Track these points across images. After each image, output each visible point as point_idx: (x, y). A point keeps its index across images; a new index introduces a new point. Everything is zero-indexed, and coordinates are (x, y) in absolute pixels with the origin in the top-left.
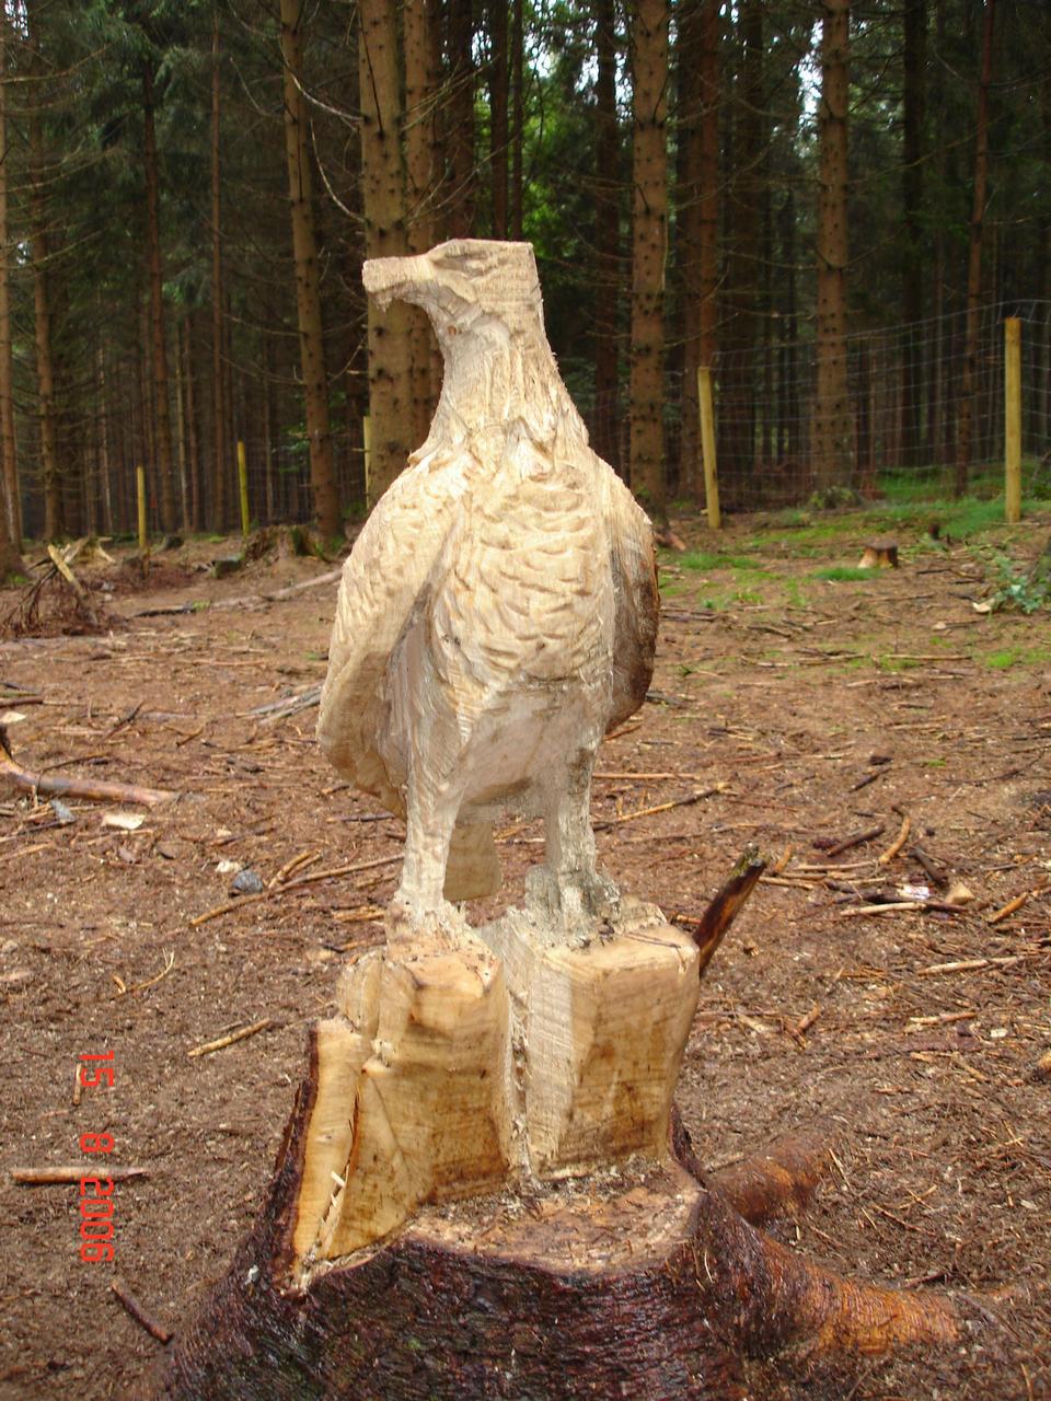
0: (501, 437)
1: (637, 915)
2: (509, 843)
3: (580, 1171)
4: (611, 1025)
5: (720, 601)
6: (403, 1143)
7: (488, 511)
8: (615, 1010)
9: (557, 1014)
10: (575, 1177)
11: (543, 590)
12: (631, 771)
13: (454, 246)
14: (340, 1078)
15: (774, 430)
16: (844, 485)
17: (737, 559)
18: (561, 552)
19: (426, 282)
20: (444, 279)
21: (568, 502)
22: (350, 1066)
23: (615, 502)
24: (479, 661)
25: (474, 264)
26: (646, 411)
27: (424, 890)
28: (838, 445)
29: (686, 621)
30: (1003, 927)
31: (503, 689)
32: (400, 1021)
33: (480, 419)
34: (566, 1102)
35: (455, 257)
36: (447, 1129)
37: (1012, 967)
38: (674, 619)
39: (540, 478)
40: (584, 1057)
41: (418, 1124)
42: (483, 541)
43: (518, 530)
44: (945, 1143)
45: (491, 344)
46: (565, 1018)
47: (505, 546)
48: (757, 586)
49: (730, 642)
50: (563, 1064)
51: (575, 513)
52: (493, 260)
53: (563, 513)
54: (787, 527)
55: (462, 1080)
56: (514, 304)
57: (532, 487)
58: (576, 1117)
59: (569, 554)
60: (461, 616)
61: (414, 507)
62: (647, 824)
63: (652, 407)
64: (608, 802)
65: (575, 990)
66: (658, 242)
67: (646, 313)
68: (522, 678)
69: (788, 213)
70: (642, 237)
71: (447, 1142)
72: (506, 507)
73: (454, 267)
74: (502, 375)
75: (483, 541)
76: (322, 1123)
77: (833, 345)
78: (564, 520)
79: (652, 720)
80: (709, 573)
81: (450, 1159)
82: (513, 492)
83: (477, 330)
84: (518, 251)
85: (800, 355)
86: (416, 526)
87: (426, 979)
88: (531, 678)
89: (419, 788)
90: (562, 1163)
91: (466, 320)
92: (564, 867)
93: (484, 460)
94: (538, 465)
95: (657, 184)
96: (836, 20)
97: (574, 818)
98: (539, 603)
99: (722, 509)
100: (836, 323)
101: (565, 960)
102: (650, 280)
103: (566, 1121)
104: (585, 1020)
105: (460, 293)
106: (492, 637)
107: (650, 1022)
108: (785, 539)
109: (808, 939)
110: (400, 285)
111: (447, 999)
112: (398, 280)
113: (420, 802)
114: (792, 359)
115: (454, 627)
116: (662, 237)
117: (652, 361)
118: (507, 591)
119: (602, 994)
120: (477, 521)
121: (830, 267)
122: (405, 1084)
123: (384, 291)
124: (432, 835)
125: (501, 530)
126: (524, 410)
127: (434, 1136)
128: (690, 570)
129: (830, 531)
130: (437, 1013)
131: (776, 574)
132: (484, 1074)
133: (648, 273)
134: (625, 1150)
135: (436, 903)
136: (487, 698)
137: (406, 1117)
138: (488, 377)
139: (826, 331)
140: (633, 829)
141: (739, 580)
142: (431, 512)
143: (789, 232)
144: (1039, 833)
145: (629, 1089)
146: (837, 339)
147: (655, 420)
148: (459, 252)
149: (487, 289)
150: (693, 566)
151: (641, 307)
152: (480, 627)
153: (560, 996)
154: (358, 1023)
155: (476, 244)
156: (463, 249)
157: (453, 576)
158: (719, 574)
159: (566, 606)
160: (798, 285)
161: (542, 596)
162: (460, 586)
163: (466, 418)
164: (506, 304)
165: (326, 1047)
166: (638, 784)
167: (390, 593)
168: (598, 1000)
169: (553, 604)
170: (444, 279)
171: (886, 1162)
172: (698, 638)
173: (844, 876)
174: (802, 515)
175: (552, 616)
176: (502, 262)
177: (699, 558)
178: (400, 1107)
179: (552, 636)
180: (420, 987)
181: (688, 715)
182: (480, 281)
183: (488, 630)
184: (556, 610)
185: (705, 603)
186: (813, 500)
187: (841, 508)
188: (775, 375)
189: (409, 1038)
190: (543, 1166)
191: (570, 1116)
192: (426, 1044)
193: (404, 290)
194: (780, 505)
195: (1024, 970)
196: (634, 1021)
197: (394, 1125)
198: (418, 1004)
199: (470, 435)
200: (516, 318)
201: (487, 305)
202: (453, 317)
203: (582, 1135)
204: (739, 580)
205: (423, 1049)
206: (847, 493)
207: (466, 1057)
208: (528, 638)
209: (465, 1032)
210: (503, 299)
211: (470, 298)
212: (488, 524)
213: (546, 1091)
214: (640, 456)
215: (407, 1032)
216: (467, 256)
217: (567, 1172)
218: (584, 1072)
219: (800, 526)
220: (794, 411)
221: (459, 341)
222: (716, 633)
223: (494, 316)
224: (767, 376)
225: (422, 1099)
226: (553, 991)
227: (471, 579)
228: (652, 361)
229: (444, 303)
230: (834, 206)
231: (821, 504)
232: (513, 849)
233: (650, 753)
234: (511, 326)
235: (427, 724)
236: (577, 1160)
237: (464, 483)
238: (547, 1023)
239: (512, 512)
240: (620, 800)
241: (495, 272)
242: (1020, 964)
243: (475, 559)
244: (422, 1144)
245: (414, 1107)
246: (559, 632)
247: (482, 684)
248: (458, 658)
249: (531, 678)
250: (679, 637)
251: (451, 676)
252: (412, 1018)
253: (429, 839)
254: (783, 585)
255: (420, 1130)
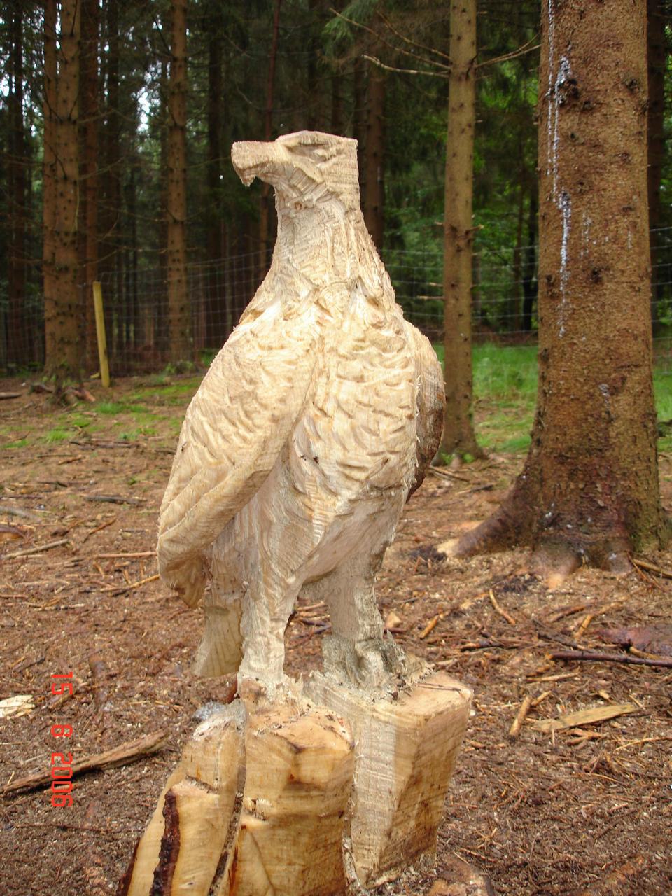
0: (346, 292)
1: (417, 667)
2: (57, 609)
3: (393, 877)
4: (424, 758)
5: (133, 435)
6: (275, 881)
7: (342, 351)
8: (428, 746)
9: (383, 755)
10: (390, 882)
11: (387, 415)
12: (123, 552)
13: (306, 136)
14: (200, 832)
15: (125, 325)
16: (186, 359)
17: (133, 406)
18: (397, 384)
19: (283, 164)
20: (297, 162)
21: (398, 346)
22: (208, 821)
23: (419, 347)
24: (332, 474)
25: (320, 152)
26: (66, 309)
27: (272, 667)
28: (183, 334)
29: (112, 448)
30: (431, 640)
31: (353, 497)
32: (279, 781)
33: (322, 275)
34: (387, 823)
35: (306, 145)
36: (313, 864)
37: (452, 667)
38: (103, 447)
39: (377, 326)
40: (403, 787)
41: (290, 864)
42: (339, 376)
43: (369, 367)
44: (484, 796)
45: (331, 217)
46: (389, 758)
47: (360, 379)
48: (152, 424)
49: (146, 462)
50: (385, 795)
51: (403, 354)
52: (333, 150)
53: (395, 353)
54: (155, 386)
55: (327, 822)
56: (348, 186)
57: (374, 332)
58: (393, 834)
59: (403, 386)
60: (319, 437)
61: (282, 347)
62: (152, 588)
63: (70, 307)
64: (117, 574)
65: (400, 735)
66: (72, 199)
67: (65, 244)
68: (368, 487)
69: (131, 188)
70: (62, 195)
71: (312, 874)
72: (357, 348)
73: (303, 154)
74: (341, 243)
75: (339, 376)
76: (185, 873)
77: (178, 270)
78: (396, 359)
79: (121, 515)
80: (117, 416)
81: (312, 888)
82: (362, 336)
83: (321, 206)
84: (349, 145)
85: (139, 277)
86: (290, 363)
87: (302, 743)
88: (373, 488)
89: (266, 582)
90: (381, 872)
91: (312, 196)
92: (361, 636)
93: (332, 311)
94: (374, 316)
95: (71, 160)
96: (178, 64)
97: (367, 597)
98: (386, 425)
99: (111, 375)
100: (180, 256)
101: (391, 712)
102: (68, 223)
103: (386, 839)
104: (406, 758)
105: (310, 174)
106: (349, 455)
107: (446, 751)
108: (157, 394)
109: (309, 660)
110: (263, 165)
111: (322, 757)
112: (262, 160)
113: (267, 594)
114: (135, 280)
115: (313, 448)
116: (76, 195)
117: (69, 276)
118: (363, 417)
119: (422, 736)
120: (332, 360)
121: (175, 221)
122: (281, 833)
123: (250, 168)
124: (276, 620)
125: (356, 366)
126: (361, 271)
127: (303, 871)
128: (103, 415)
129: (185, 388)
130: (314, 770)
131: (161, 416)
132: (341, 814)
133: (66, 219)
134: (417, 853)
135: (279, 677)
136: (340, 505)
137: (279, 859)
138: (329, 244)
139: (174, 261)
140: (144, 593)
141: (138, 421)
142: (301, 352)
143: (132, 198)
144: (420, 576)
145: (426, 805)
146: (181, 266)
147: (72, 316)
148: (310, 141)
149: (330, 173)
150: (105, 412)
151: (61, 240)
152: (337, 447)
153: (386, 740)
154: (216, 784)
155: (322, 136)
156: (313, 139)
157: (311, 405)
158: (124, 417)
159: (402, 428)
160: (138, 233)
161: (388, 420)
162: (319, 413)
163: (312, 277)
164: (344, 186)
165: (184, 808)
166: (134, 560)
167: (275, 420)
168: (418, 740)
169: (394, 427)
170: (297, 162)
171: (455, 816)
172: (124, 459)
173: (309, 614)
174: (165, 378)
175: (393, 436)
176: (339, 152)
177: (109, 406)
178: (275, 853)
179: (393, 452)
180: (298, 750)
181: (145, 511)
182: (324, 166)
183: (345, 448)
184: (395, 431)
185: (122, 435)
186: (168, 369)
187: (188, 374)
188: (124, 290)
189: (286, 794)
190: (369, 878)
191: (389, 835)
192: (302, 797)
193: (265, 170)
194: (147, 372)
195: (460, 668)
196: (436, 753)
197: (269, 867)
198: (297, 765)
199: (316, 290)
200: (349, 197)
201: (330, 185)
202: (302, 194)
203: (395, 848)
204: (138, 421)
205: (298, 801)
206: (190, 364)
207: (332, 803)
208: (375, 454)
209: (336, 782)
210: (341, 182)
211: (318, 179)
212: (343, 361)
213: (370, 817)
214: (62, 339)
215: (285, 789)
216: (316, 145)
217: (384, 879)
218: (403, 797)
219: (164, 385)
220: (136, 311)
221: (303, 214)
222: (135, 454)
223: (334, 195)
224: (120, 291)
225: (295, 843)
226: (380, 738)
227: (330, 407)
228: (69, 276)
229: (293, 182)
230: (178, 182)
231: (173, 371)
232: (62, 613)
233: (131, 539)
234: (347, 203)
235: (277, 529)
236: (390, 868)
237: (318, 328)
238: (373, 764)
239: (362, 352)
240: (126, 572)
241: (334, 160)
242: (456, 665)
243: (334, 391)
244: (293, 879)
245: (287, 851)
246: (397, 449)
247: (335, 494)
248: (316, 472)
249: (373, 488)
250: (111, 459)
251: (309, 488)
252: (292, 777)
253: (274, 624)
254: (169, 423)
255: (291, 868)
